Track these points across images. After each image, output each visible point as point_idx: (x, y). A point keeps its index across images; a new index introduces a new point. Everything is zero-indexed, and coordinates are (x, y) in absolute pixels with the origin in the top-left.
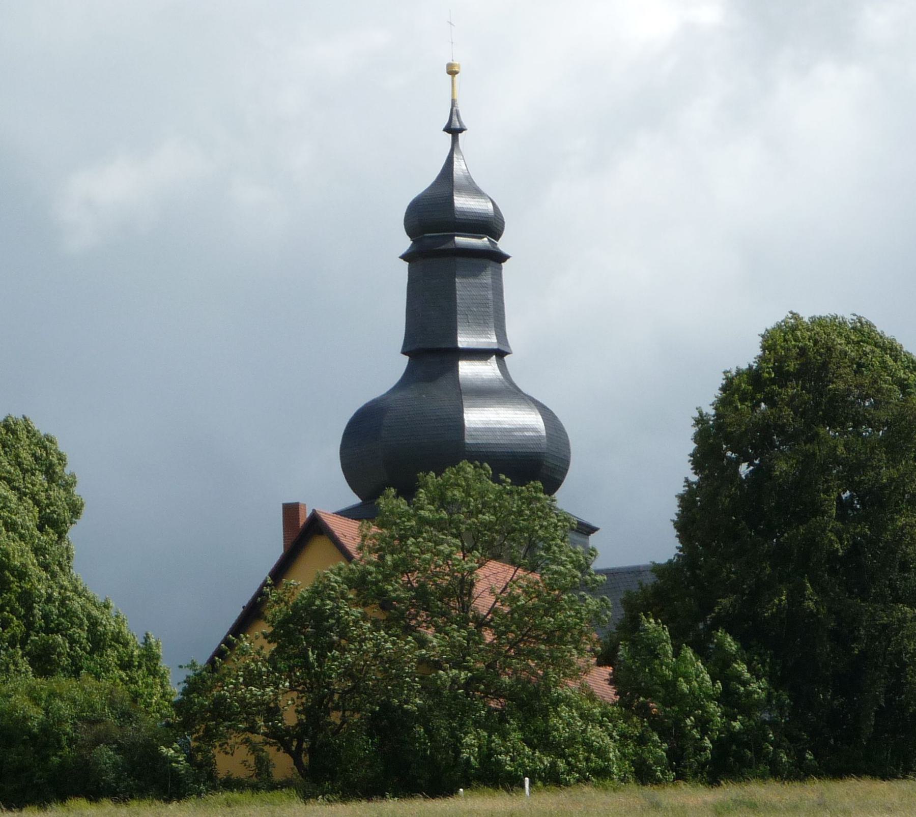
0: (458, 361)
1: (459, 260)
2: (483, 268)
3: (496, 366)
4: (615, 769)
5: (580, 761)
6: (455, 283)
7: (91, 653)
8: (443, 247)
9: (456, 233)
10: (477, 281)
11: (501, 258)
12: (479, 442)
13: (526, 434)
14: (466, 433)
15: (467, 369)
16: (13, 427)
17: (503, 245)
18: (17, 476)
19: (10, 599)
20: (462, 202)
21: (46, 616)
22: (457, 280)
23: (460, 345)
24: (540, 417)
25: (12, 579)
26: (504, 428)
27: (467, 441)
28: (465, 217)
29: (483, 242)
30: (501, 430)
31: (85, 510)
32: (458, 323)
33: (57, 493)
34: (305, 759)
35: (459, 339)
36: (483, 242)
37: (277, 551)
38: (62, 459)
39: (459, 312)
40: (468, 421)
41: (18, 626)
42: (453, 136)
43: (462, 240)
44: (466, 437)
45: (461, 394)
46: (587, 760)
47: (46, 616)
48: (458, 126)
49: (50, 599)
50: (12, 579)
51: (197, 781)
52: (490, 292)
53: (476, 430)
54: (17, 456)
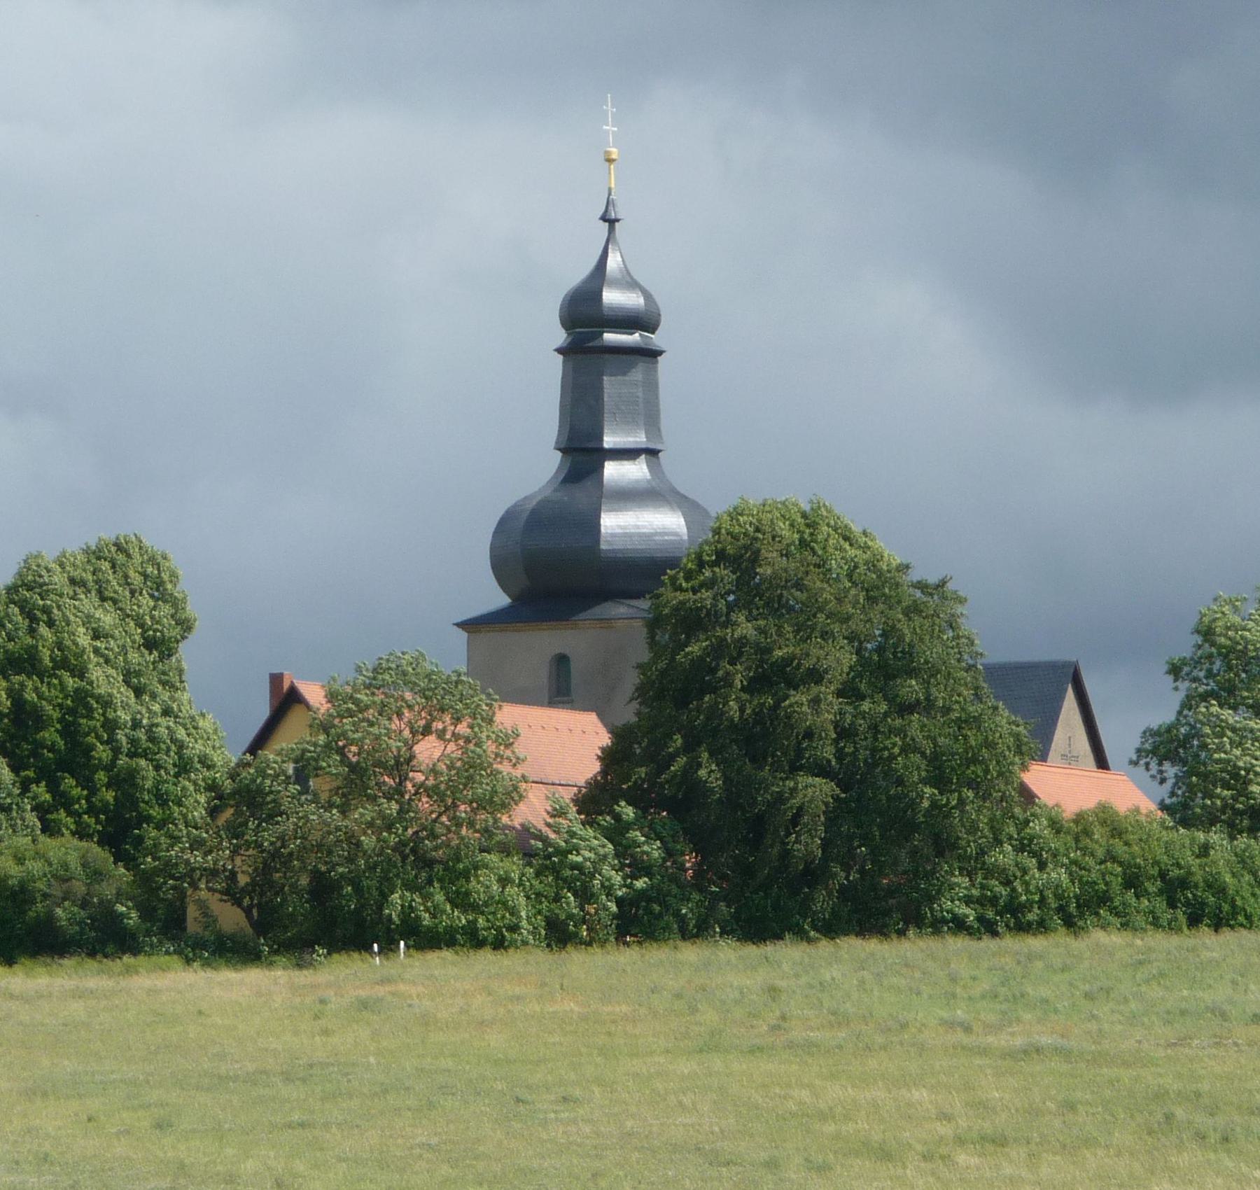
0: (604, 462)
1: (607, 356)
2: (632, 366)
3: (644, 467)
4: (524, 923)
5: (497, 920)
6: (603, 380)
7: (177, 775)
8: (590, 344)
9: (605, 329)
10: (627, 378)
11: (652, 354)
12: (615, 547)
13: (666, 538)
14: (602, 539)
15: (613, 471)
16: (125, 546)
17: (657, 339)
18: (124, 597)
19: (95, 727)
20: (612, 297)
21: (133, 742)
22: (605, 378)
23: (606, 446)
24: (682, 520)
25: (95, 706)
26: (643, 533)
27: (603, 546)
28: (613, 313)
29: (633, 338)
30: (640, 535)
31: (195, 632)
32: (606, 423)
33: (165, 610)
34: (255, 912)
35: (605, 439)
36: (633, 338)
37: (263, 712)
38: (174, 576)
39: (606, 411)
40: (605, 526)
41: (104, 751)
42: (609, 226)
43: (610, 337)
44: (602, 542)
45: (602, 497)
46: (503, 917)
47: (133, 742)
48: (613, 216)
49: (136, 725)
50: (95, 706)
51: (148, 933)
52: (641, 389)
53: (613, 535)
54: (126, 577)
